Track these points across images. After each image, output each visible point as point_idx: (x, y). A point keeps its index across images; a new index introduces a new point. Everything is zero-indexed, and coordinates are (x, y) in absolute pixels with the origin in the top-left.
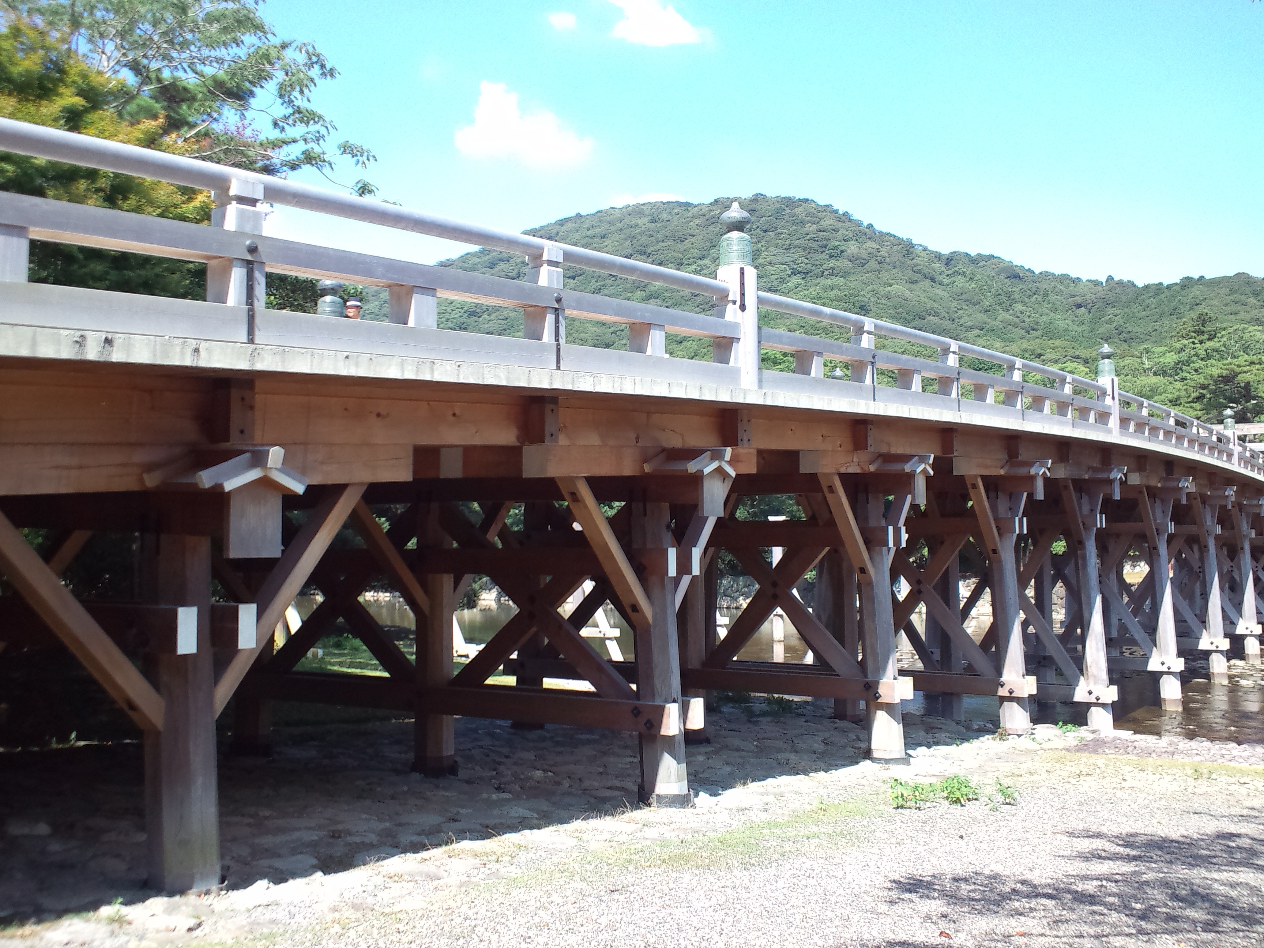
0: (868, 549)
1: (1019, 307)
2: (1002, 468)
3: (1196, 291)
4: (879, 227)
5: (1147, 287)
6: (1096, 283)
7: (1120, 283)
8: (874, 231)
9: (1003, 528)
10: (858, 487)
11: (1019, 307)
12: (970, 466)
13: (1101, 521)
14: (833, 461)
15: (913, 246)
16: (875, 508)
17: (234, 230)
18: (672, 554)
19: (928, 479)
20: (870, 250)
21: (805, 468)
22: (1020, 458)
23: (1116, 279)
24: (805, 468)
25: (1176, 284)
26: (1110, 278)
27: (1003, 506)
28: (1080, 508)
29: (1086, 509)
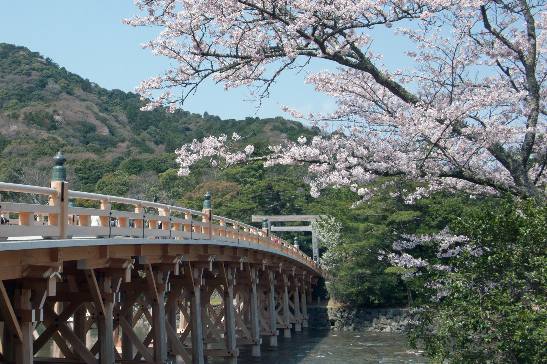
0: (104, 303)
1: (152, 128)
2: (160, 259)
3: (253, 126)
4: (69, 69)
5: (227, 121)
6: (198, 116)
7: (212, 117)
8: (66, 71)
9: (160, 288)
10: (101, 274)
11: (152, 128)
12: (148, 260)
13: (203, 282)
14: (91, 265)
15: (90, 83)
16: (108, 283)
17: (45, 329)
18: (34, 311)
19: (132, 270)
20: (63, 85)
21: (79, 268)
22: (169, 254)
23: (210, 114)
24: (79, 268)
25: (243, 121)
26: (206, 114)
27: (160, 276)
28: (193, 274)
29: (196, 276)
